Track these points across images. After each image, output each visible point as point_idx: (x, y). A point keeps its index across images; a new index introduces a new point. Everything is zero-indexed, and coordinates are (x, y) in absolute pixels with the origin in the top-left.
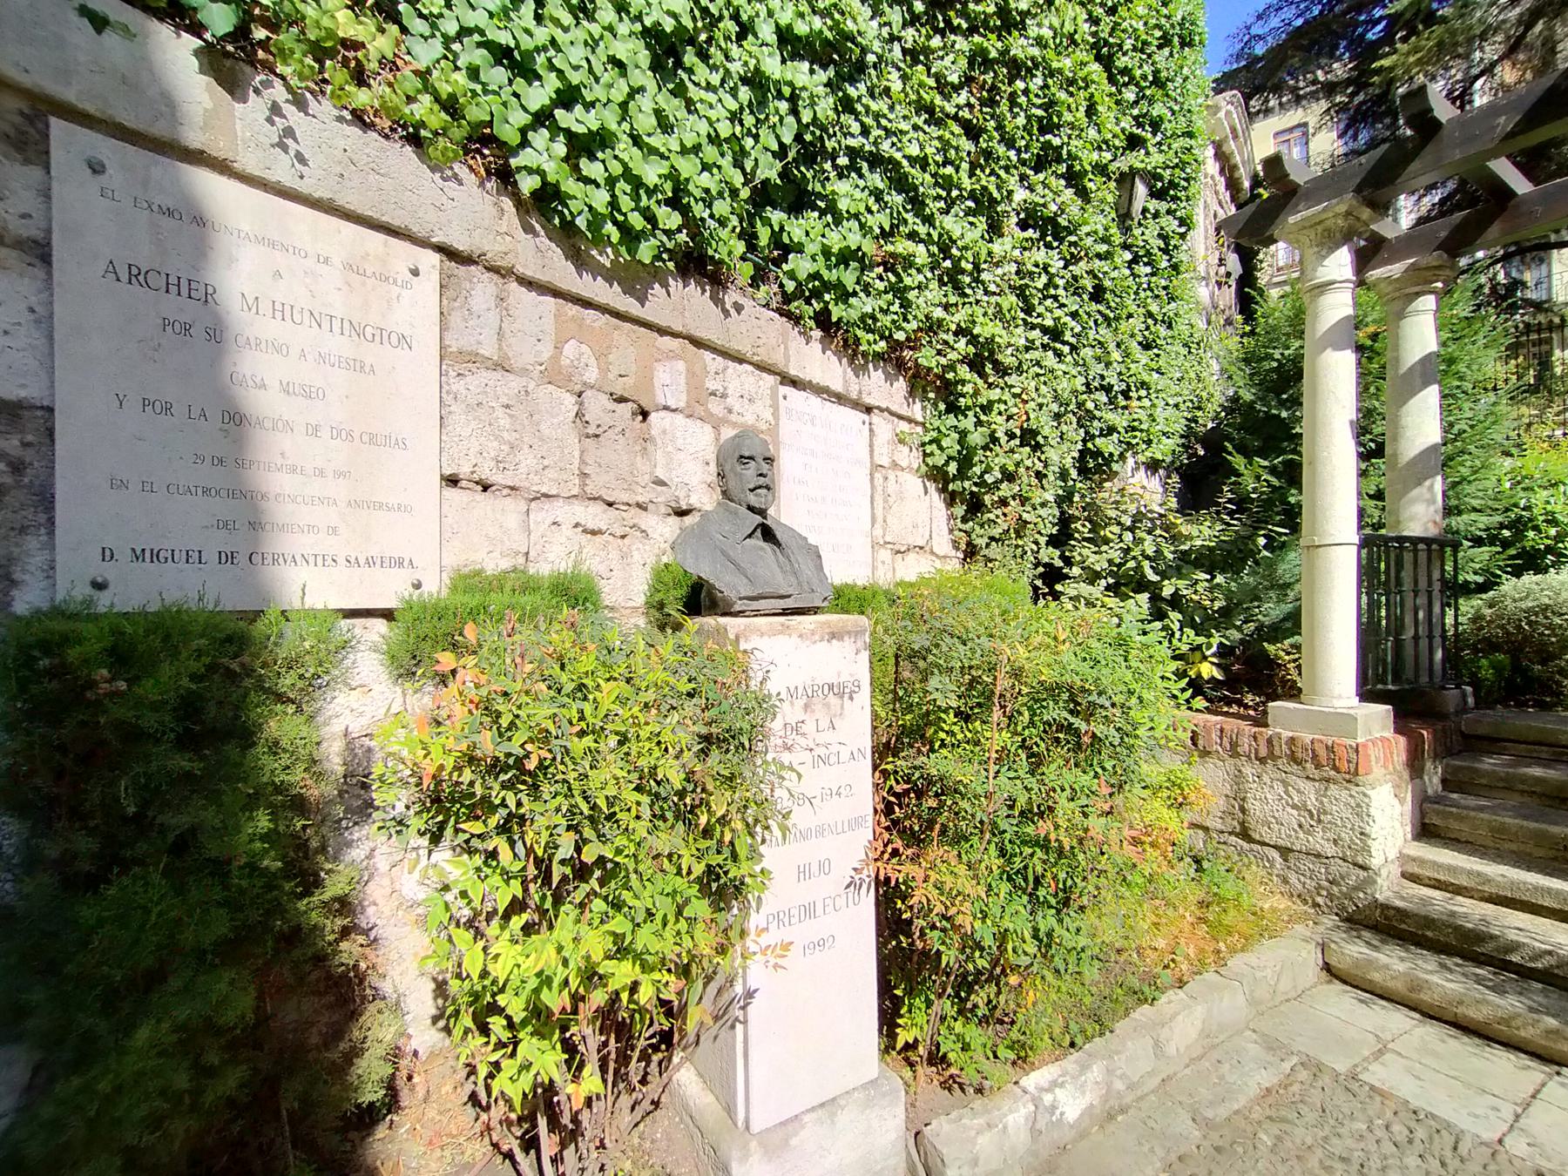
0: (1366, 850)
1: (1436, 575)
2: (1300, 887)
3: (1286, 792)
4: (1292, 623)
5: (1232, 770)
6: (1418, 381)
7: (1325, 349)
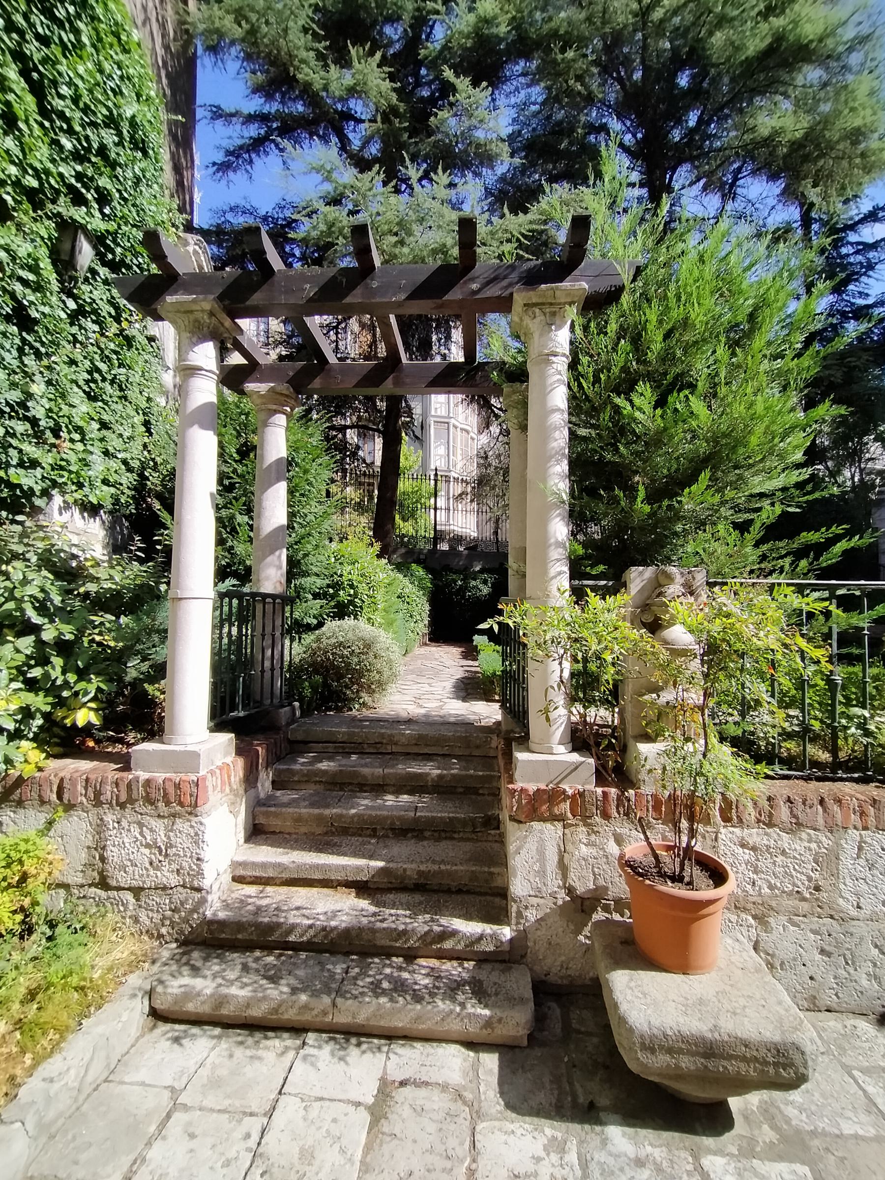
0: (200, 874)
1: (278, 622)
2: (148, 923)
3: (141, 834)
4: (159, 671)
5: (95, 820)
6: (273, 475)
7: (192, 425)
